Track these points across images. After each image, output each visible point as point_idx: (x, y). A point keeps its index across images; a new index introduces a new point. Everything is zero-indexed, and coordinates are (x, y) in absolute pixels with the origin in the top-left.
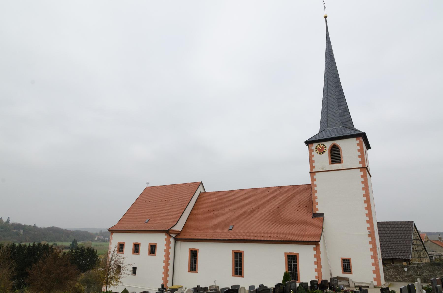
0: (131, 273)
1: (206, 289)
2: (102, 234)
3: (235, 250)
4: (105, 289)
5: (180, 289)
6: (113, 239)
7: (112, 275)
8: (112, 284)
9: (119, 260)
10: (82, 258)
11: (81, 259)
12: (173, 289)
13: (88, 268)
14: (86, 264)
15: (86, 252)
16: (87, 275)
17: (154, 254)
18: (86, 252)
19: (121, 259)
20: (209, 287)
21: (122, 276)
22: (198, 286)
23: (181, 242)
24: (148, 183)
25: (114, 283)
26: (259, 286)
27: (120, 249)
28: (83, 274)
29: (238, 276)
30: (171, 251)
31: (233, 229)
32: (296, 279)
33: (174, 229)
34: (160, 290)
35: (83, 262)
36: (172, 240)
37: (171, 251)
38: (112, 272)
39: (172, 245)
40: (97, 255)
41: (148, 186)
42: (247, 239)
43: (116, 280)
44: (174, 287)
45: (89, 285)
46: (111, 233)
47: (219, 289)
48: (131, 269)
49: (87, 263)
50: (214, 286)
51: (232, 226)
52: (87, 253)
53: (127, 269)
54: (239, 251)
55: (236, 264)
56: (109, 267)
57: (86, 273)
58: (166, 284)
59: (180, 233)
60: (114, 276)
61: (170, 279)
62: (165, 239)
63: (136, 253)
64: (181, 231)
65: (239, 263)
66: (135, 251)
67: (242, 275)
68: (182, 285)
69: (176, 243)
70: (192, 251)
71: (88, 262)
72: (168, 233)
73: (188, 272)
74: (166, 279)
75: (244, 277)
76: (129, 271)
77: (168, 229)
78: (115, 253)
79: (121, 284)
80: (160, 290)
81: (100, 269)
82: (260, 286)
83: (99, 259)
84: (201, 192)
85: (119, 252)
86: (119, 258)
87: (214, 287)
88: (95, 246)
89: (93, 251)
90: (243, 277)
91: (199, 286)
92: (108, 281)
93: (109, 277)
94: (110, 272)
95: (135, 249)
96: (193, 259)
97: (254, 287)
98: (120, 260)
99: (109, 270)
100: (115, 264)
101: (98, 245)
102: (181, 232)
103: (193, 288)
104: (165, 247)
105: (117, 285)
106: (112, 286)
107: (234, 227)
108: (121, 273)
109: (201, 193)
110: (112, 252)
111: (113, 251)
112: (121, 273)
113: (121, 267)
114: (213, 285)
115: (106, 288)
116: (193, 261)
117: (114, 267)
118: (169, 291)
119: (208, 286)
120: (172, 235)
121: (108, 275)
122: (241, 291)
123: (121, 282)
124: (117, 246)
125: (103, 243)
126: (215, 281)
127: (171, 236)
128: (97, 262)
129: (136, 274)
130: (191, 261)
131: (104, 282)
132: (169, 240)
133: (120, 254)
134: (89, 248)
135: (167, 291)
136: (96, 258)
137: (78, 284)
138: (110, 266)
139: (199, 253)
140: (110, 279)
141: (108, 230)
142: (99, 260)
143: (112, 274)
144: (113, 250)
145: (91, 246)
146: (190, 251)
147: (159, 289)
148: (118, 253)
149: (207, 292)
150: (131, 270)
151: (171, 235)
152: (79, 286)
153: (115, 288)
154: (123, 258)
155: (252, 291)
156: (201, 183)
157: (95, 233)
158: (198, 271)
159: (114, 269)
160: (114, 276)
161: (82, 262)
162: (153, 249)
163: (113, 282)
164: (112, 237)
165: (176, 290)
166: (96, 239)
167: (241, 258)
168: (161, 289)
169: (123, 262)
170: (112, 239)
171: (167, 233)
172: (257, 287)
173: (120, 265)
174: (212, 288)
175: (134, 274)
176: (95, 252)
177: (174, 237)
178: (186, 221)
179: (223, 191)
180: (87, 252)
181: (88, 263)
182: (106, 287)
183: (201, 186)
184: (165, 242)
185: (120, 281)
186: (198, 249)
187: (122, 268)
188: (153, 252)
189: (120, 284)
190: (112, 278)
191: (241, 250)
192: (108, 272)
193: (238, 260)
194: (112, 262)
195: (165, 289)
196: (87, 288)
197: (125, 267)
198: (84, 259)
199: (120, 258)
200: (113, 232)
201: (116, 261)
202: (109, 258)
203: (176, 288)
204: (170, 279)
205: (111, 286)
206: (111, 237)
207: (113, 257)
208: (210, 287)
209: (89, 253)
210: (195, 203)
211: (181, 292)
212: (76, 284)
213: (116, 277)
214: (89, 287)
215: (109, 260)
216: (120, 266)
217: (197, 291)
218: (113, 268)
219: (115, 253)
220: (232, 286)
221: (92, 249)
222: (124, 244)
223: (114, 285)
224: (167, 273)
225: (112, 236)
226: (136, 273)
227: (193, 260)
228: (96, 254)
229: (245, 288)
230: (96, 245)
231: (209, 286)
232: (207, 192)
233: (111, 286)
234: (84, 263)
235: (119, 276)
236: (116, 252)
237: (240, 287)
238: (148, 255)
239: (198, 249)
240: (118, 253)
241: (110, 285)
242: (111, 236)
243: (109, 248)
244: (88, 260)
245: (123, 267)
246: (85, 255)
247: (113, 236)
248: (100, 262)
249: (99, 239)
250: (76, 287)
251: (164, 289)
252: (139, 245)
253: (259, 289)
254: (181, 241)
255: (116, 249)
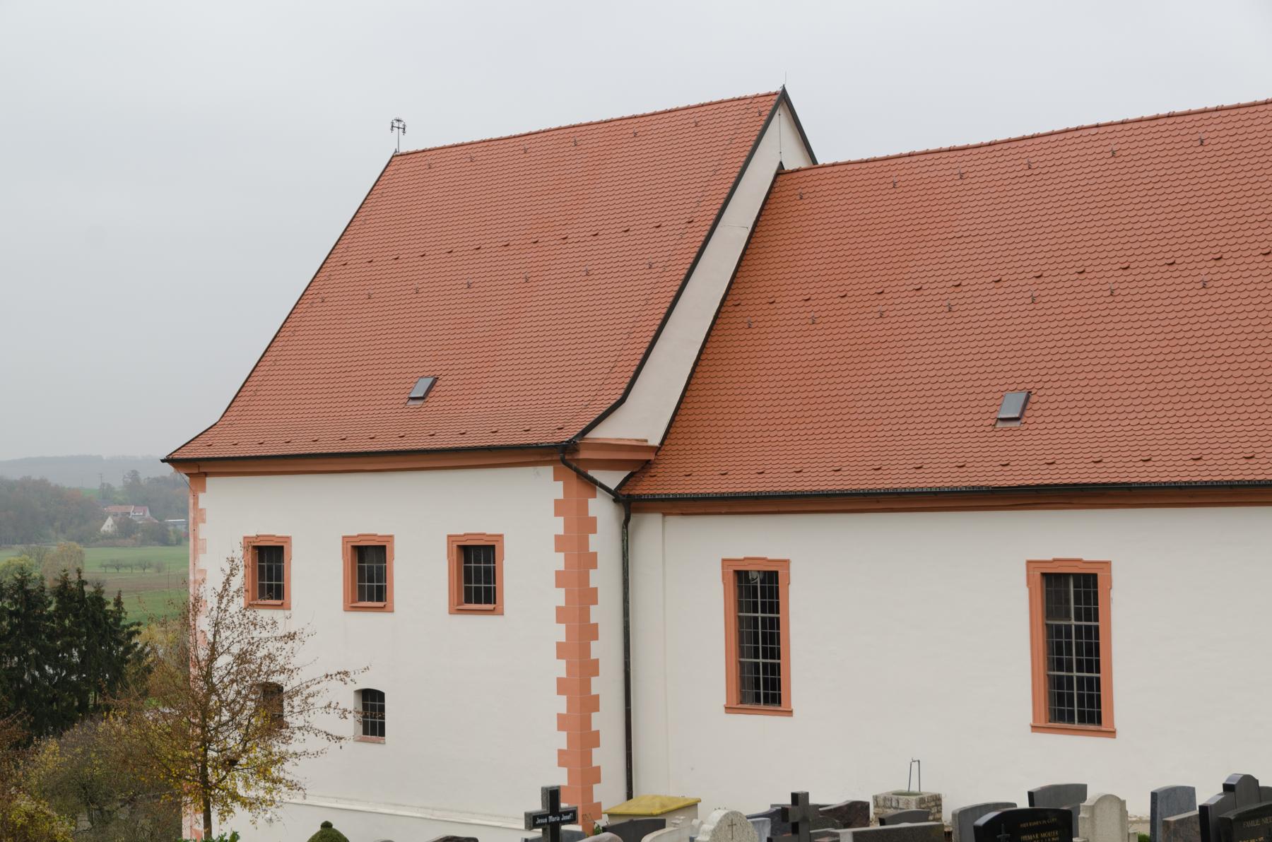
0: (351, 726)
1: (853, 813)
2: (137, 491)
3: (742, 557)
4: (196, 827)
5: (679, 819)
6: (208, 517)
7: (231, 743)
8: (235, 797)
9: (261, 653)
10: (34, 645)
11: (24, 651)
12: (631, 821)
13: (83, 707)
14: (64, 680)
15: (52, 608)
16: (78, 750)
17: (488, 601)
18: (52, 608)
19: (279, 645)
20: (877, 806)
21: (294, 746)
22: (795, 797)
23: (664, 522)
24: (398, 125)
25: (252, 794)
26: (1222, 791)
27: (261, 577)
28: (52, 745)
29: (1076, 725)
30: (605, 578)
31: (1027, 413)
32: (1061, 713)
33: (607, 432)
34: (539, 821)
35: (42, 671)
36: (602, 510)
37: (605, 578)
38: (226, 723)
39: (604, 541)
40: (128, 627)
41: (403, 150)
42: (1185, 478)
43: (262, 771)
44: (642, 806)
45: (100, 809)
46: (187, 478)
47: (947, 817)
48: (350, 702)
49: (69, 674)
50: (909, 794)
51: (1023, 396)
52: (61, 614)
53: (320, 702)
54: (1079, 560)
55: (1059, 652)
56: (207, 696)
57: (73, 736)
58: (588, 793)
59: (652, 457)
60: (244, 751)
61: (608, 757)
62: (557, 501)
63: (371, 599)
64: (662, 443)
65: (1079, 646)
66: (361, 588)
67: (1100, 722)
68: (691, 796)
69: (630, 525)
70: (747, 572)
71: (71, 669)
72: (570, 466)
73: (729, 709)
74: (587, 757)
75: (795, 713)
76: (334, 715)
77: (565, 437)
78: (233, 608)
79: (297, 797)
80: (539, 821)
81: (156, 714)
82: (1228, 788)
83: (143, 649)
84: (787, 167)
85: (260, 602)
86: (265, 634)
87: (908, 803)
88: (110, 570)
89: (98, 600)
90: (1112, 733)
91: (807, 795)
92: (213, 779)
93: (215, 754)
94: (212, 724)
95: (361, 579)
96: (756, 627)
97: (1189, 792)
98: (272, 647)
99: (206, 713)
100: (238, 672)
101: (125, 567)
102: (656, 450)
103: (766, 808)
104: (562, 555)
105: (273, 802)
106: (237, 807)
107: (1033, 399)
108: (286, 732)
109: (781, 171)
110: (212, 602)
111: (221, 597)
112: (288, 728)
113: (285, 689)
114: (905, 789)
115: (202, 822)
116: (756, 642)
117: (239, 693)
118: (605, 829)
119: (866, 797)
120: (597, 475)
121: (206, 742)
122: (1093, 826)
123: (292, 786)
124: (240, 562)
125: (154, 552)
126: (915, 765)
127: (593, 484)
128: (130, 669)
129: (382, 733)
130: (741, 640)
131: (186, 786)
132: (584, 507)
133: (265, 615)
134: (65, 583)
135: (596, 832)
136: (120, 643)
137: (25, 803)
138: (212, 689)
139: (791, 587)
140: (224, 768)
141: (169, 469)
142: (140, 656)
143: (233, 740)
144: (219, 589)
145: (79, 572)
146: (731, 577)
147: (527, 815)
148: (250, 606)
149: (855, 834)
150: (351, 707)
151: (593, 473)
152: (37, 816)
153: (260, 821)
154: (291, 637)
155: (1172, 819)
156: (783, 99)
157: (96, 486)
158: (794, 706)
159: (237, 707)
160: (244, 751)
161: (37, 673)
162: (478, 570)
163: (240, 784)
164: (201, 505)
165: (656, 823)
166: (108, 526)
167: (1088, 611)
168: (542, 816)
169: (295, 662)
170: (204, 521)
171: (564, 462)
172: (1208, 793)
173: (274, 679)
174: (895, 808)
175: (373, 733)
176: (110, 607)
177: (613, 486)
178: (691, 377)
179: (946, 146)
180: (57, 609)
181: (74, 678)
182: (200, 817)
183: (780, 124)
184: (558, 526)
185: (288, 777)
186: (787, 562)
187: (290, 697)
188: (478, 590)
189: (286, 799)
190: (232, 763)
191: (1087, 557)
192: (204, 727)
193: (1073, 622)
194: (222, 661)
195: (568, 817)
196: (88, 825)
197: (310, 690)
198: (48, 655)
199: (267, 640)
200: (206, 474)
201: (242, 658)
202: (200, 636)
203: (657, 811)
204: (608, 757)
205: (230, 811)
206: (196, 504)
207: (224, 633)
208: (881, 803)
209: (76, 616)
210: (746, 248)
211: (687, 834)
212: (13, 804)
213: (258, 753)
214: (103, 819)
215: (203, 653)
216: (279, 689)
217: (795, 828)
218: (233, 701)
219: (233, 608)
220: (1031, 795)
221: (87, 589)
222: (281, 548)
223: (248, 804)
224: (586, 722)
225: (201, 496)
226: (382, 725)
227: (756, 634)
228: (120, 619)
229: (1123, 803)
230: (111, 566)
231: (876, 798)
232: (824, 166)
233: (230, 811)
234: (51, 678)
235: (275, 750)
236: (240, 602)
237: (1092, 794)
238: (451, 613)
239: (787, 562)
240: (250, 606)
241: (225, 804)
242: (191, 501)
243: (191, 578)
244: (76, 659)
245: (297, 693)
246: (53, 628)
247: (204, 500)
248: (149, 670)
249: (126, 530)
250: (19, 821)
251: (560, 815)
252: (384, 547)
253: (1219, 805)
254: (665, 514)
255: (237, 582)
